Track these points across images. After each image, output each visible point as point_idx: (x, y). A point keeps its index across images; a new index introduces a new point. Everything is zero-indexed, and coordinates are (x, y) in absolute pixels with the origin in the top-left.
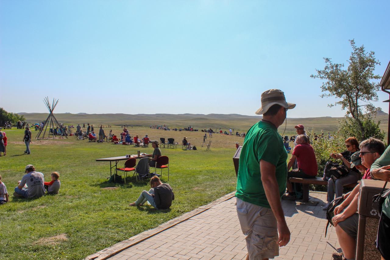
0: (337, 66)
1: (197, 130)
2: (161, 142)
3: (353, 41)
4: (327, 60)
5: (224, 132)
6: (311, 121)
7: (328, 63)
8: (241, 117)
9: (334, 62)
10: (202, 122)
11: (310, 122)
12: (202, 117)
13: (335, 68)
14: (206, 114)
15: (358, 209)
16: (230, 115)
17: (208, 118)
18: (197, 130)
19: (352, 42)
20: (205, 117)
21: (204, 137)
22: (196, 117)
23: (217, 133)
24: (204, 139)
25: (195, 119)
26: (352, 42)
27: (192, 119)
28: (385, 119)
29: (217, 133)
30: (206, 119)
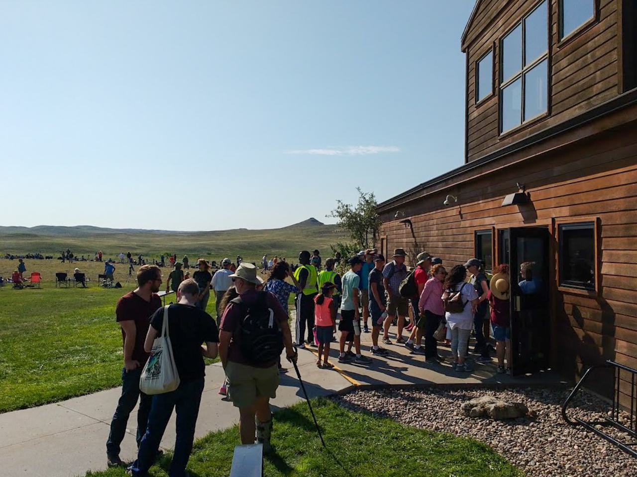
0: (347, 206)
1: (51, 258)
2: (57, 279)
3: (359, 188)
4: (339, 201)
5: (45, 258)
6: (218, 236)
7: (340, 204)
8: (106, 232)
9: (345, 203)
10: (29, 241)
11: (218, 237)
12: (24, 233)
13: (345, 208)
14: (30, 227)
15: (556, 237)
16: (78, 228)
17: (40, 234)
18: (51, 258)
19: (359, 189)
20: (28, 233)
21: (130, 268)
22: (11, 232)
23: (92, 260)
24: (130, 271)
25: (12, 237)
26: (359, 189)
27: (6, 237)
28: (321, 231)
29: (92, 260)
30: (36, 236)
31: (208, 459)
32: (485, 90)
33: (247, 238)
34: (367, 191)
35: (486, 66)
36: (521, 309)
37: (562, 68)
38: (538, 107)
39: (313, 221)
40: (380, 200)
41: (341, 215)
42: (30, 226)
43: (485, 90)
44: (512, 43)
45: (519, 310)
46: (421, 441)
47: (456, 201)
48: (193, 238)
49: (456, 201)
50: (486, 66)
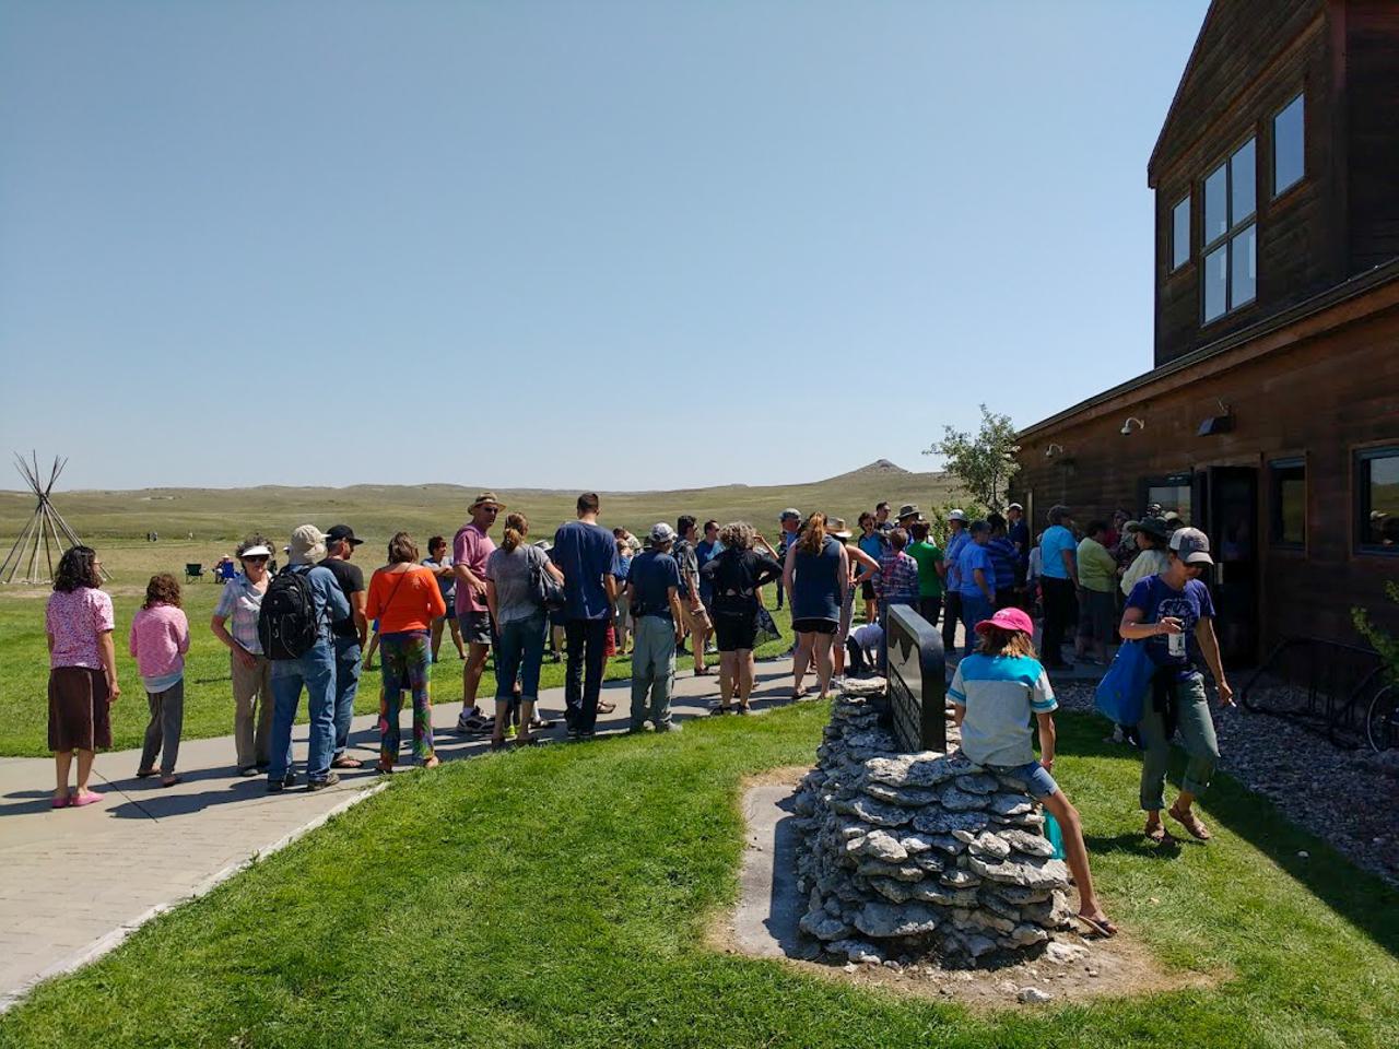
9: (958, 430)
31: (393, 982)
32: (1182, 255)
33: (749, 505)
34: (998, 410)
35: (1182, 212)
36: (1225, 581)
37: (51, 552)
38: (1245, 293)
39: (884, 465)
40: (1020, 424)
41: (949, 452)
42: (338, 485)
43: (1182, 255)
44: (1215, 183)
45: (1221, 581)
46: (655, 1020)
47: (1142, 426)
48: (642, 505)
49: (1142, 426)
50: (1182, 212)
